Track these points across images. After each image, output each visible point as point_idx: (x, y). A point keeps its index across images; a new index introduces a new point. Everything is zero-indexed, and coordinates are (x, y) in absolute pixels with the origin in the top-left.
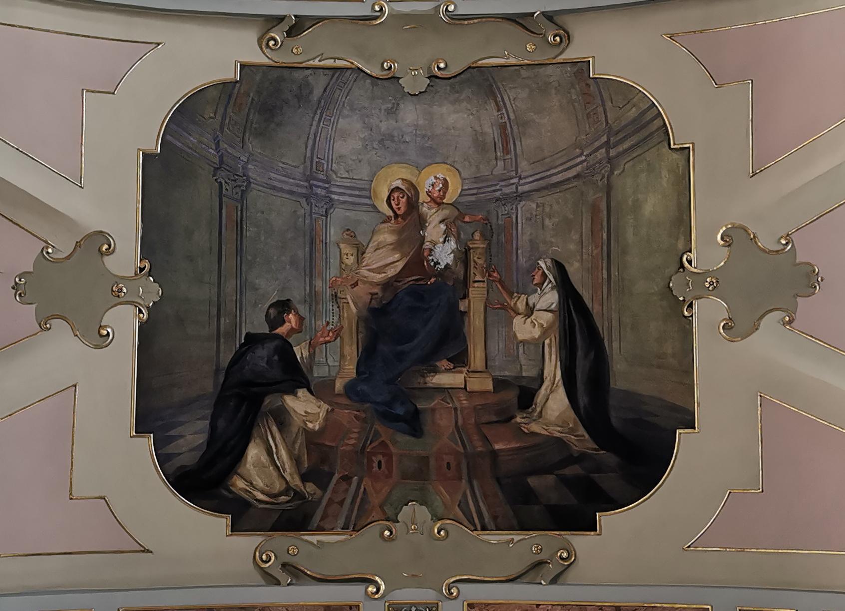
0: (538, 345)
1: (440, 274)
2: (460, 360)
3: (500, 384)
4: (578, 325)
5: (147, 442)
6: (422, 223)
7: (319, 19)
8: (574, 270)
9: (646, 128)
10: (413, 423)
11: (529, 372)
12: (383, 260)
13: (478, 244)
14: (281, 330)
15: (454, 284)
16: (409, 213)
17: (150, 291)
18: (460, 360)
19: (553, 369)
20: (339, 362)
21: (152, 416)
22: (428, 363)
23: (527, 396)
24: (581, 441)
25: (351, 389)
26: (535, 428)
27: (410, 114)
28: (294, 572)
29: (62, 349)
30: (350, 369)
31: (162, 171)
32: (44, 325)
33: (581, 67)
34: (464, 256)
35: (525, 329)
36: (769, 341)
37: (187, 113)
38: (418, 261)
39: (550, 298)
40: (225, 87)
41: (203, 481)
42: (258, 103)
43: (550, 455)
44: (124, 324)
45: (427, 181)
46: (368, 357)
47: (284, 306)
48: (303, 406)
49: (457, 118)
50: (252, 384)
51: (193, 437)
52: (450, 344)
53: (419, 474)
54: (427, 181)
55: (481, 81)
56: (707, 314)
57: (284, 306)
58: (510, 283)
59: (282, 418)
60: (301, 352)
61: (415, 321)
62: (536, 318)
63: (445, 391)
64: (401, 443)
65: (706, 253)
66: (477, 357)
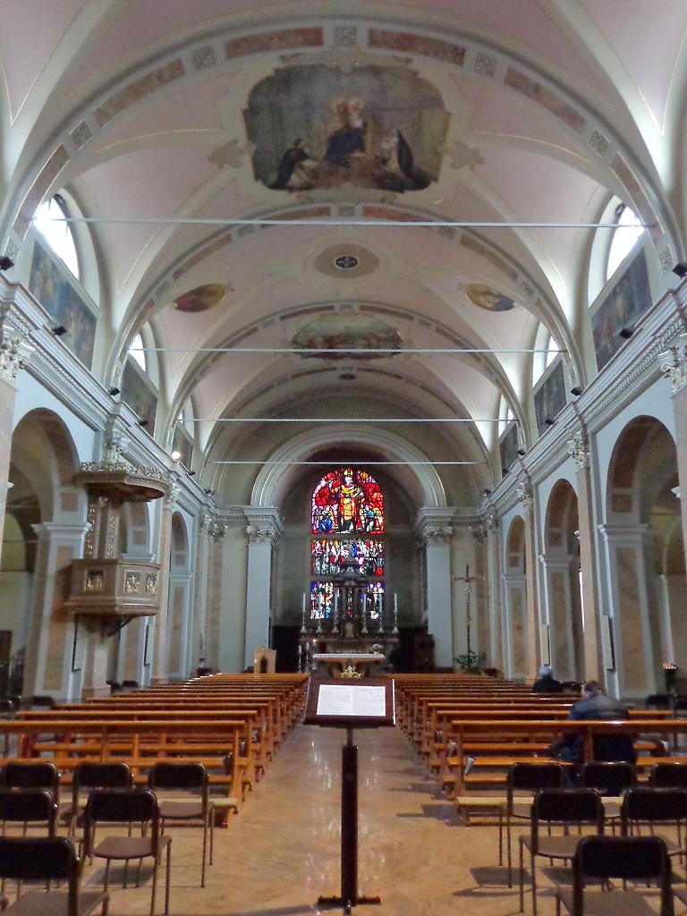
0: (390, 152)
1: (356, 129)
2: (363, 150)
3: (376, 158)
4: (404, 151)
5: (259, 183)
6: (349, 114)
7: (377, 202)
8: (406, 136)
9: (436, 101)
10: (346, 165)
11: (386, 156)
12: (336, 125)
13: (370, 123)
14: (299, 147)
15: (359, 133)
16: (345, 112)
17: (254, 147)
18: (363, 150)
19: (394, 156)
20: (322, 151)
21: (259, 175)
22: (352, 149)
23: (385, 161)
24: (402, 175)
25: (325, 158)
26: (387, 169)
27: (344, 81)
28: (311, 201)
29: (228, 171)
30: (324, 153)
31: (251, 113)
32: (221, 167)
33: (415, 73)
34: (365, 124)
35: (385, 146)
36: (464, 173)
37: (256, 91)
38: (348, 125)
39: (394, 140)
40: (268, 79)
41: (280, 184)
42: (284, 80)
43: (393, 176)
44: (247, 160)
45: (352, 102)
46: (328, 153)
47: (298, 141)
48: (308, 163)
49: (366, 83)
50: (291, 161)
51: (273, 177)
52: (360, 146)
53: (347, 178)
54: (352, 102)
55: (375, 71)
56: (447, 159)
57: (298, 141)
58: (381, 132)
59: (302, 168)
60: (306, 151)
61: (344, 143)
62: (390, 144)
63: (358, 159)
64: (342, 169)
65: (449, 145)
66: (369, 150)
